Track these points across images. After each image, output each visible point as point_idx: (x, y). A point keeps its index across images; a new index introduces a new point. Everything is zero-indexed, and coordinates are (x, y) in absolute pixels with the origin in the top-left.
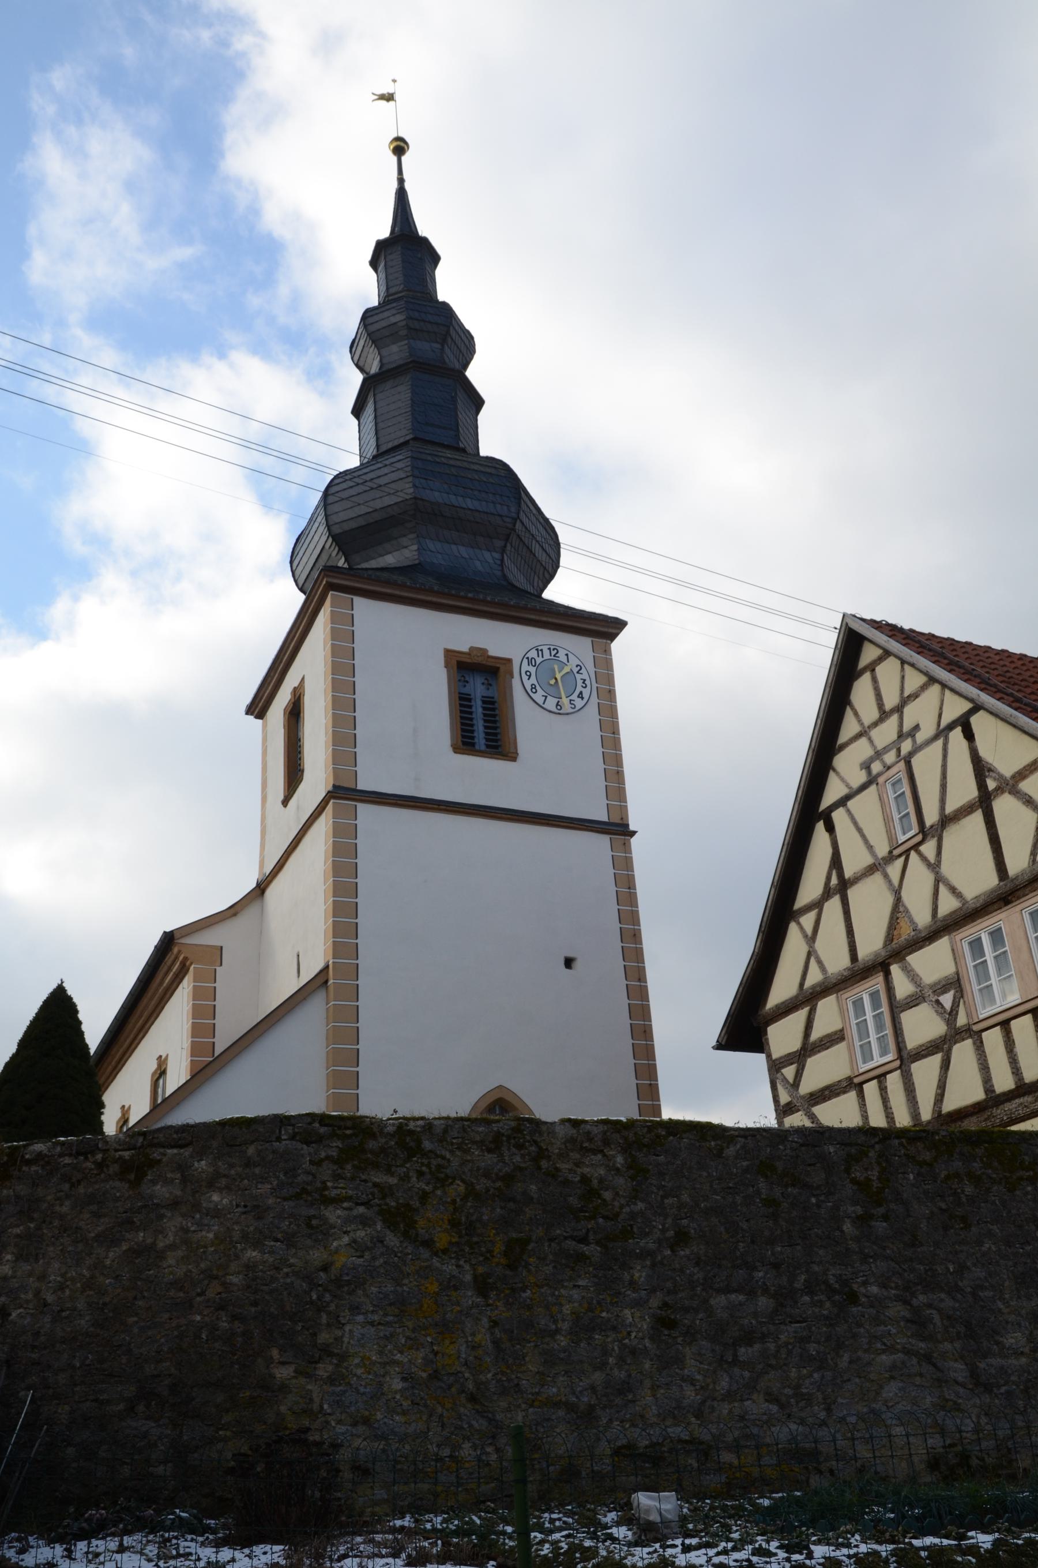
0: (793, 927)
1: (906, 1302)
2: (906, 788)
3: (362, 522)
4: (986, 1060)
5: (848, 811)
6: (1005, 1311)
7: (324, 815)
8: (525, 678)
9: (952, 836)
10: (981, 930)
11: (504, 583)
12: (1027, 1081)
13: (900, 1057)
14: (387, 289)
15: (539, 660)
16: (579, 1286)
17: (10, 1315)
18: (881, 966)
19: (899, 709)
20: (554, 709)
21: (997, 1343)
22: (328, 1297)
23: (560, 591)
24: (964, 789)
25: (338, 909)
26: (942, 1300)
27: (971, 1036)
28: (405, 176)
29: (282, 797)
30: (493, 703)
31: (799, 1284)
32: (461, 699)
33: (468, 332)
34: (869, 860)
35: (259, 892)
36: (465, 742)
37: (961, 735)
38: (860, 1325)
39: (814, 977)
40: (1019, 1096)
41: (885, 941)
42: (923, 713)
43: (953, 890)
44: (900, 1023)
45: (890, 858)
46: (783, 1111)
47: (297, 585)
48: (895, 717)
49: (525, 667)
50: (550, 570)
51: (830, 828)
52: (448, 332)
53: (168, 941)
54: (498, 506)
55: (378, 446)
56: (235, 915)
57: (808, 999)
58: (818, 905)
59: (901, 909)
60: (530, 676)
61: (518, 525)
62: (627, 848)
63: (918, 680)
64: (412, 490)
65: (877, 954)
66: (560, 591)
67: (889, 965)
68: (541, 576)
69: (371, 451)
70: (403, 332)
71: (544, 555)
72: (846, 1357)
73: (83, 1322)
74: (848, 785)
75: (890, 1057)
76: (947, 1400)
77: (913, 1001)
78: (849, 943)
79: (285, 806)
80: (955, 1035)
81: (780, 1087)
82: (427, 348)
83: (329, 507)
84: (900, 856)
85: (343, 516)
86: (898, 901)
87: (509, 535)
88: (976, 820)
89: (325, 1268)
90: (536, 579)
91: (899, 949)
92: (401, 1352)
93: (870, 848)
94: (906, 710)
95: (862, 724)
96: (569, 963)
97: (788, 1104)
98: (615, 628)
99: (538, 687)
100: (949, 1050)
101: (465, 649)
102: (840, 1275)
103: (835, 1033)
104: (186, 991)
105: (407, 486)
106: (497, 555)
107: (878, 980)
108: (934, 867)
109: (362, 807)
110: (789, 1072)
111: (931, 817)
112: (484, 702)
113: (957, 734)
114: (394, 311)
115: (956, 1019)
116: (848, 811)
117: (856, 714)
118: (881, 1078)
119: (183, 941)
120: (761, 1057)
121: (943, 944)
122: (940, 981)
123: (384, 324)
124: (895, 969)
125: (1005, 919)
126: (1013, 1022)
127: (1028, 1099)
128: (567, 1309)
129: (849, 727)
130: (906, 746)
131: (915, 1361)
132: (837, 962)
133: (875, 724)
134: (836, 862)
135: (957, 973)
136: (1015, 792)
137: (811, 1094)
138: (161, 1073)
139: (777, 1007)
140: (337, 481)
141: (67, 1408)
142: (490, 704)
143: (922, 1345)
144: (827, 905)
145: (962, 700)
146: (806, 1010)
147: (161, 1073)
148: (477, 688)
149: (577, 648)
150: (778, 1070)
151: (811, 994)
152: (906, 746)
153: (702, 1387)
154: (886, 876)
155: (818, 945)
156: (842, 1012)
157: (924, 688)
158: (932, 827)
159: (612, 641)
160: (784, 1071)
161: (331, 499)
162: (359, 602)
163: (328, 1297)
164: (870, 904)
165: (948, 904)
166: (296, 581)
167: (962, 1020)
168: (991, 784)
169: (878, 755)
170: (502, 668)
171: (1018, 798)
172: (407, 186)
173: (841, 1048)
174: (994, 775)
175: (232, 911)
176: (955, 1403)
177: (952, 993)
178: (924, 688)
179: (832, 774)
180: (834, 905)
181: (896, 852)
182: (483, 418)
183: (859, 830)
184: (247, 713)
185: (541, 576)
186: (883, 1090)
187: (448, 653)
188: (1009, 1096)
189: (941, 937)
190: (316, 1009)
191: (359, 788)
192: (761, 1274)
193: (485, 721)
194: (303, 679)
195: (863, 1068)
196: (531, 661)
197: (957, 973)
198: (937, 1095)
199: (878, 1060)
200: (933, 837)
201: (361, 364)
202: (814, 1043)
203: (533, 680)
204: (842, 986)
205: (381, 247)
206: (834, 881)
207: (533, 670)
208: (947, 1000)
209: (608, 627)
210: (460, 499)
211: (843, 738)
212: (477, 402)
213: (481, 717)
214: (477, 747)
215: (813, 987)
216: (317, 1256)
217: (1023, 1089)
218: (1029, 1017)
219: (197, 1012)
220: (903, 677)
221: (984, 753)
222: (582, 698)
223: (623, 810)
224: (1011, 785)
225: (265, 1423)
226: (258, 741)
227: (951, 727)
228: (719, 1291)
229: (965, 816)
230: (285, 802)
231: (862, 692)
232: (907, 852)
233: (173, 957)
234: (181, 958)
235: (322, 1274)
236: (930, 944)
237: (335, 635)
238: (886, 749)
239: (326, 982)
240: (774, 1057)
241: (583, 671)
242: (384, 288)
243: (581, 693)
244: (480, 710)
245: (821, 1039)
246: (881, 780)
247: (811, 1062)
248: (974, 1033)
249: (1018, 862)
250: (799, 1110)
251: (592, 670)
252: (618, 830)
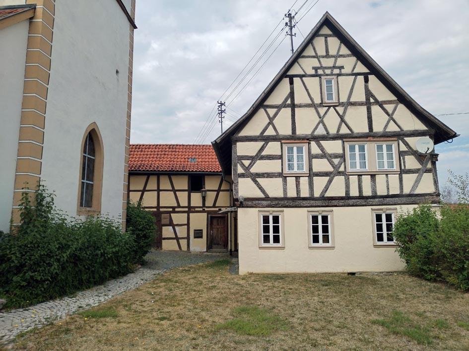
7: (223, 184)
58: (279, 108)
88: (177, 193)
232: (329, 107)
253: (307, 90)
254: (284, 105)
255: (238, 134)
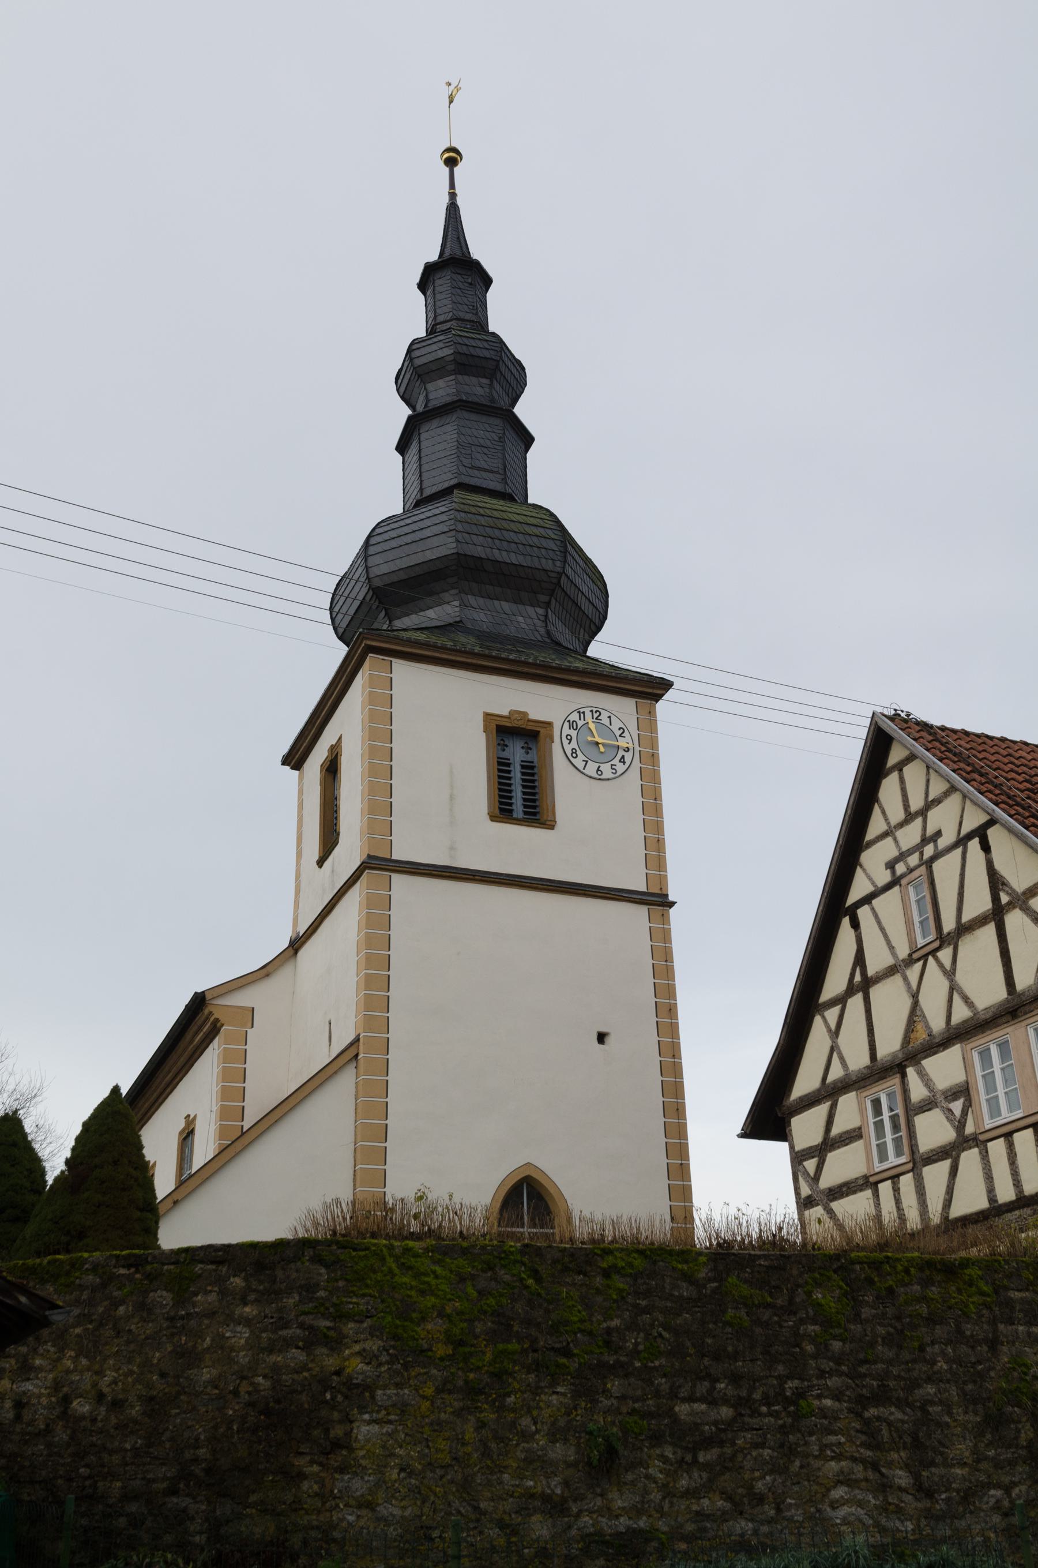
0: (818, 1020)
1: (859, 1415)
2: (926, 892)
3: (403, 576)
4: (990, 1170)
5: (873, 909)
6: (953, 1424)
7: (358, 884)
8: (565, 742)
9: (968, 946)
10: (991, 1042)
11: (547, 640)
12: (1026, 1194)
13: (913, 1160)
14: (435, 317)
15: (580, 723)
16: (557, 1393)
17: (71, 1403)
18: (897, 1067)
19: (923, 812)
20: (595, 775)
21: (942, 1454)
22: (340, 1398)
23: (604, 649)
24: (979, 901)
25: (369, 982)
26: (892, 1413)
27: (977, 1146)
28: (458, 190)
29: (317, 858)
30: (532, 768)
31: (757, 1396)
32: (499, 763)
33: (519, 362)
34: (890, 961)
35: (291, 951)
36: (502, 811)
37: (978, 846)
38: (811, 1434)
39: (836, 1073)
40: (1019, 1208)
41: (903, 1044)
42: (946, 819)
43: (966, 1000)
44: (914, 1126)
45: (910, 961)
46: (805, 1203)
47: (336, 633)
48: (919, 821)
49: (566, 730)
50: (597, 622)
51: (855, 925)
52: (497, 367)
53: (199, 1003)
54: (543, 561)
55: (421, 490)
56: (268, 975)
57: (829, 1093)
58: (841, 1001)
59: (918, 1013)
60: (570, 740)
61: (563, 579)
62: (665, 919)
63: (937, 788)
64: (454, 545)
65: (894, 1055)
66: (604, 649)
67: (905, 1067)
68: (587, 629)
69: (414, 495)
70: (451, 367)
71: (591, 607)
72: (797, 1463)
73: (133, 1412)
74: (873, 883)
75: (903, 1159)
76: (890, 1504)
77: (927, 1106)
78: (869, 1042)
79: (320, 867)
80: (963, 1142)
81: (801, 1179)
82: (477, 388)
83: (370, 559)
84: (919, 960)
85: (385, 569)
86: (916, 1004)
87: (553, 590)
88: (989, 931)
89: (338, 1373)
90: (582, 631)
91: (916, 1051)
92: (401, 1447)
93: (891, 948)
94: (930, 814)
95: (888, 824)
96: (601, 1038)
97: (809, 1197)
98: (660, 689)
99: (579, 752)
100: (958, 1156)
101: (505, 712)
102: (797, 1388)
103: (854, 1130)
104: (217, 1052)
105: (450, 540)
106: (541, 611)
107: (896, 1080)
108: (950, 974)
109: (396, 878)
110: (810, 1165)
111: (949, 925)
112: (523, 767)
113: (974, 844)
114: (441, 345)
115: (964, 1126)
116: (873, 909)
117: (884, 813)
118: (895, 1178)
119: (215, 1002)
120: (784, 1146)
121: (955, 1051)
122: (951, 1088)
123: (430, 358)
124: (910, 1071)
125: (1012, 1033)
126: (1015, 1135)
127: (1028, 1211)
128: (546, 1413)
129: (876, 825)
130: (929, 851)
131: (861, 1468)
132: (858, 1059)
133: (901, 825)
134: (860, 959)
135: (967, 1082)
136: (1027, 910)
137: (830, 1190)
138: (187, 1135)
139: (801, 1099)
140: (378, 531)
141: (119, 1484)
142: (529, 769)
143: (869, 1453)
144: (850, 1001)
145: (980, 811)
146: (828, 1104)
147: (187, 1135)
148: (517, 753)
149: (621, 710)
150: (800, 1163)
151: (833, 1089)
152: (929, 851)
153: (663, 1485)
154: (905, 979)
155: (841, 1040)
156: (862, 1110)
157: (947, 794)
158: (949, 934)
159: (657, 701)
160: (805, 1163)
161: (372, 550)
162: (399, 665)
163: (340, 1398)
164: (890, 1002)
165: (961, 1013)
166: (335, 629)
167: (970, 1129)
168: (1004, 899)
169: (902, 856)
170: (543, 731)
171: (1028, 915)
172: (459, 201)
173: (858, 1145)
174: (1007, 889)
175: (264, 971)
176: (897, 1506)
177: (962, 1100)
178: (947, 794)
179: (859, 870)
180: (856, 1002)
181: (915, 956)
182: (533, 456)
183: (882, 929)
184: (283, 764)
185: (587, 629)
186: (896, 1190)
187: (487, 716)
188: (1010, 1207)
189: (954, 1045)
190: (346, 1082)
191: (394, 858)
192: (723, 1386)
193: (524, 787)
194: (340, 738)
195: (878, 1167)
196: (572, 725)
197: (967, 1082)
198: (945, 1200)
199: (893, 1160)
200: (949, 944)
201: (406, 396)
202: (834, 1139)
203: (574, 744)
204: (862, 1083)
205: (430, 272)
206: (858, 978)
207: (574, 733)
208: (957, 1106)
209: (654, 688)
210: (504, 553)
211: (870, 835)
212: (527, 439)
213: (520, 790)
214: (515, 815)
215: (835, 1082)
216: (331, 1362)
217: (1023, 1201)
218: (1030, 1131)
219: (226, 1075)
220: (928, 781)
221: (998, 866)
222: (624, 763)
223: (663, 879)
224: (1020, 902)
225: (284, 1503)
226: (293, 794)
227: (969, 836)
228: (684, 1400)
229: (980, 927)
230: (320, 863)
231: (889, 790)
232: (925, 958)
233: (204, 1017)
234: (212, 1019)
235: (335, 1377)
236: (944, 1050)
237: (372, 699)
238: (910, 852)
239: (357, 1055)
240: (797, 1149)
241: (626, 734)
242: (431, 315)
243: (623, 757)
244: (519, 775)
245: (841, 1135)
246: (904, 882)
247: (831, 1157)
248: (979, 1142)
249: (1023, 980)
250: (818, 1205)
251: (635, 733)
252: (657, 901)
253: (882, 929)
254: (851, 990)
255: (789, 1095)
